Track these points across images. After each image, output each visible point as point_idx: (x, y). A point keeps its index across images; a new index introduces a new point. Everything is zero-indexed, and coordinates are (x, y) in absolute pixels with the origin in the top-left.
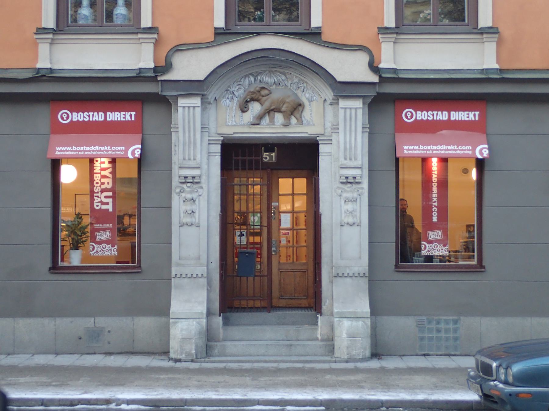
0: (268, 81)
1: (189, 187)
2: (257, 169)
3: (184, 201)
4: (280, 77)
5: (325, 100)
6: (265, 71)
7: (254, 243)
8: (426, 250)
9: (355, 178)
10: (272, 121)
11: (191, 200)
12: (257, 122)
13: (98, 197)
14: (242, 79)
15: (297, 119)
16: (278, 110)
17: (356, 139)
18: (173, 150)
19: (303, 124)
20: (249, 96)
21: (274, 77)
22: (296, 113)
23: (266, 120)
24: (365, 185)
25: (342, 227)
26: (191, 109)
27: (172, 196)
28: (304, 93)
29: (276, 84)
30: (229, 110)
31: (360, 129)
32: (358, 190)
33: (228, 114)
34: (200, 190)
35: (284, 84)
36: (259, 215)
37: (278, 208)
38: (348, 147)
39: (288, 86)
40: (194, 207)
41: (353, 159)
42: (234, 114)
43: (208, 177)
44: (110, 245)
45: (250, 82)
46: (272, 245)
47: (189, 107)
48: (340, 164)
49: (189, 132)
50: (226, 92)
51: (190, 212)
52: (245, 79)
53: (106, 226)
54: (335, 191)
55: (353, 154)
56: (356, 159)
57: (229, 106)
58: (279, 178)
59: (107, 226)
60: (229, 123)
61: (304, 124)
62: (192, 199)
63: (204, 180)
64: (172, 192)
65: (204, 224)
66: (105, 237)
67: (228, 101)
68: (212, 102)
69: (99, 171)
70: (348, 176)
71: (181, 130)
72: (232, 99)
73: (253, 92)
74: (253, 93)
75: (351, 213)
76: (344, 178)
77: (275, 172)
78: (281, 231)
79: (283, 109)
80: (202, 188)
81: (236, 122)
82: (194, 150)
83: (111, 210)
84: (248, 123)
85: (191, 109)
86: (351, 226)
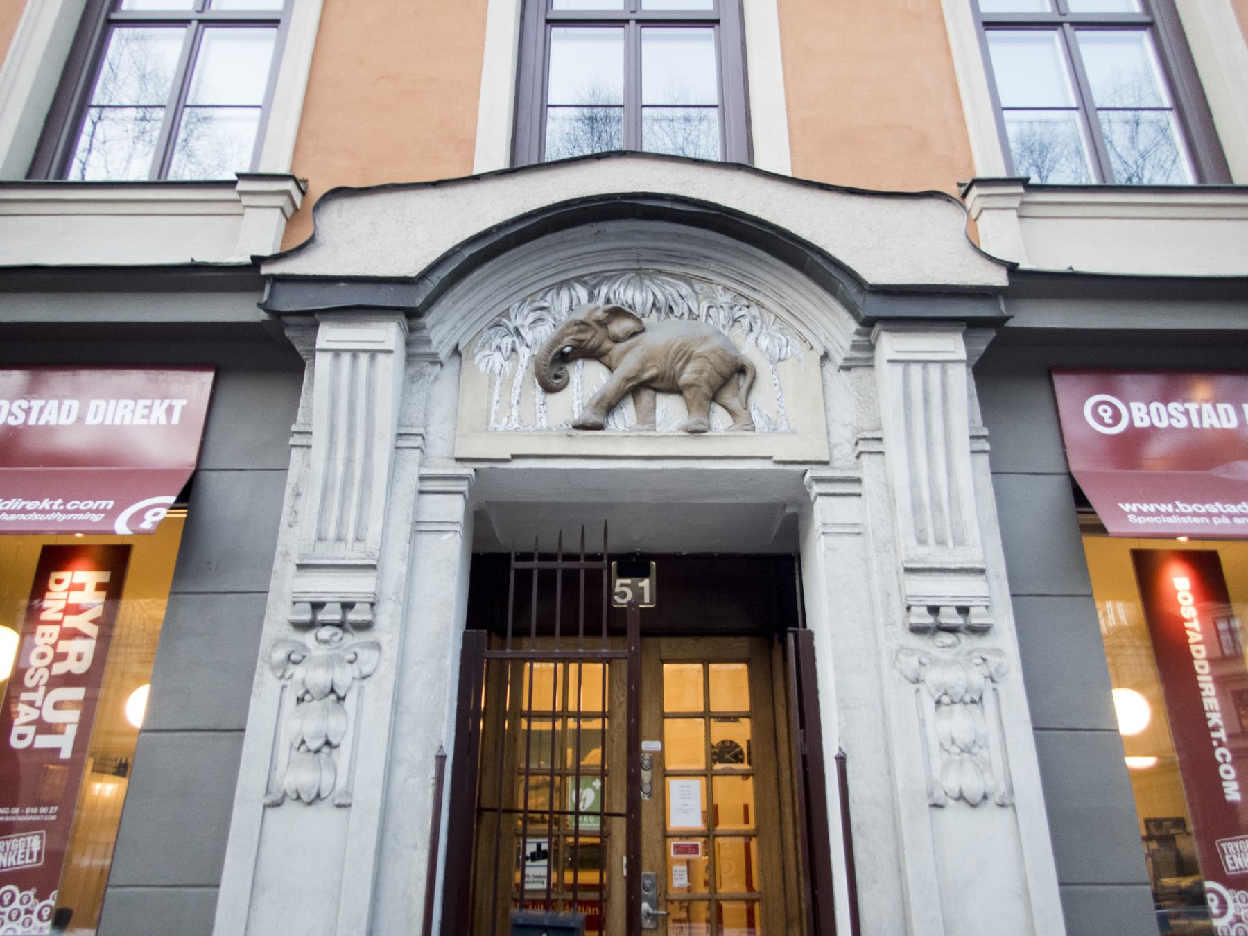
0: (633, 299)
1: (326, 642)
2: (593, 631)
3: (300, 700)
4: (671, 287)
5: (825, 357)
7: (575, 887)
8: (1229, 916)
9: (963, 611)
10: (647, 418)
11: (326, 696)
12: (593, 419)
13: (31, 704)
14: (551, 292)
15: (732, 413)
16: (666, 384)
17: (950, 472)
18: (286, 509)
19: (754, 429)
21: (656, 288)
22: (728, 396)
23: (627, 414)
24: (1005, 637)
25: (935, 810)
26: (364, 359)
27: (256, 678)
28: (753, 336)
29: (659, 310)
31: (962, 442)
32: (984, 660)
33: (496, 397)
34: (364, 655)
35: (685, 306)
36: (597, 783)
37: (660, 757)
38: (926, 498)
39: (698, 316)
40: (336, 725)
41: (950, 542)
43: (407, 609)
44: (31, 893)
46: (640, 891)
47: (355, 353)
48: (904, 558)
49: (351, 443)
50: (492, 331)
51: (314, 745)
52: (558, 294)
53: (33, 814)
54: (895, 661)
55: (948, 522)
56: (959, 542)
58: (663, 661)
59: (38, 814)
60: (497, 426)
62: (332, 691)
63: (386, 618)
64: (259, 663)
65: (368, 797)
66: (20, 856)
67: (498, 358)
68: (442, 356)
69: (59, 616)
70: (937, 603)
71: (319, 441)
72: (514, 353)
73: (582, 323)
74: (583, 327)
75: (966, 750)
76: (925, 610)
77: (651, 641)
78: (672, 843)
79: (687, 377)
80: (377, 646)
81: (521, 422)
82: (361, 506)
83: (66, 754)
84: (565, 426)
85: (364, 359)
86: (973, 806)
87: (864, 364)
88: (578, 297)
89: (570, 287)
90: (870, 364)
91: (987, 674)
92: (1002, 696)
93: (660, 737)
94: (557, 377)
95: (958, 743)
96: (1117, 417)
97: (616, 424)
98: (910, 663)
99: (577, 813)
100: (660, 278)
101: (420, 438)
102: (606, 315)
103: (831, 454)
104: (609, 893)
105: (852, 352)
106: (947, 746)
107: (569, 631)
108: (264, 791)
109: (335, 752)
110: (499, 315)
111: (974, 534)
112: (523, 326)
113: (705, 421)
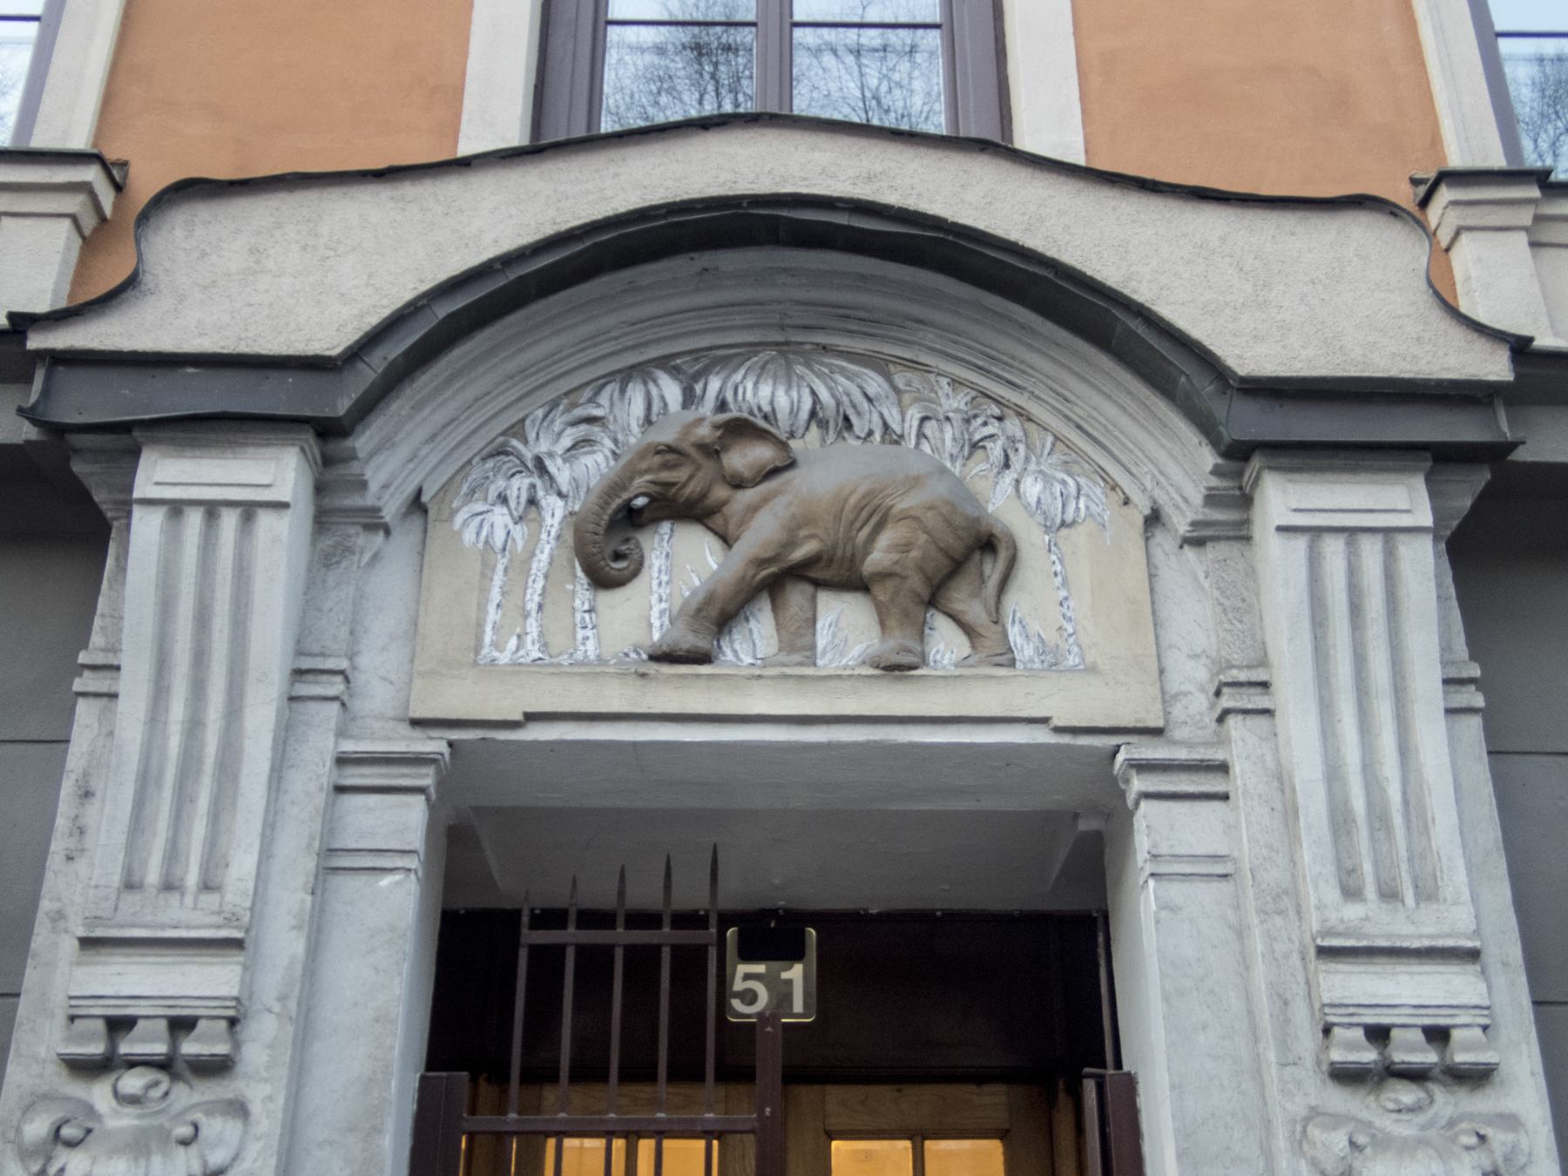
0: (772, 403)
1: (133, 1100)
2: (686, 1072)
4: (848, 378)
5: (1154, 519)
6: (755, 347)
9: (1438, 1035)
12: (689, 640)
14: (609, 388)
17: (1405, 751)
18: (61, 823)
19: (1012, 663)
20: (648, 477)
22: (961, 597)
26: (229, 521)
28: (1009, 477)
29: (823, 425)
30: (506, 570)
32: (1482, 1138)
33: (495, 595)
34: (214, 1127)
38: (1359, 805)
42: (537, 599)
45: (656, 408)
47: (212, 509)
48: (1315, 927)
50: (490, 464)
52: (623, 391)
54: (1300, 1141)
56: (1427, 893)
57: (504, 549)
58: (831, 1136)
60: (496, 654)
61: (1018, 664)
71: (134, 684)
72: (533, 508)
73: (670, 449)
74: (671, 457)
76: (1359, 1034)
79: (879, 557)
80: (239, 1109)
81: (545, 646)
82: (215, 817)
84: (633, 655)
85: (229, 521)
87: (1231, 533)
88: (663, 398)
90: (1244, 533)
94: (618, 556)
97: (735, 652)
100: (827, 360)
101: (339, 679)
102: (718, 433)
105: (1207, 511)
111: (1456, 878)
113: (915, 645)
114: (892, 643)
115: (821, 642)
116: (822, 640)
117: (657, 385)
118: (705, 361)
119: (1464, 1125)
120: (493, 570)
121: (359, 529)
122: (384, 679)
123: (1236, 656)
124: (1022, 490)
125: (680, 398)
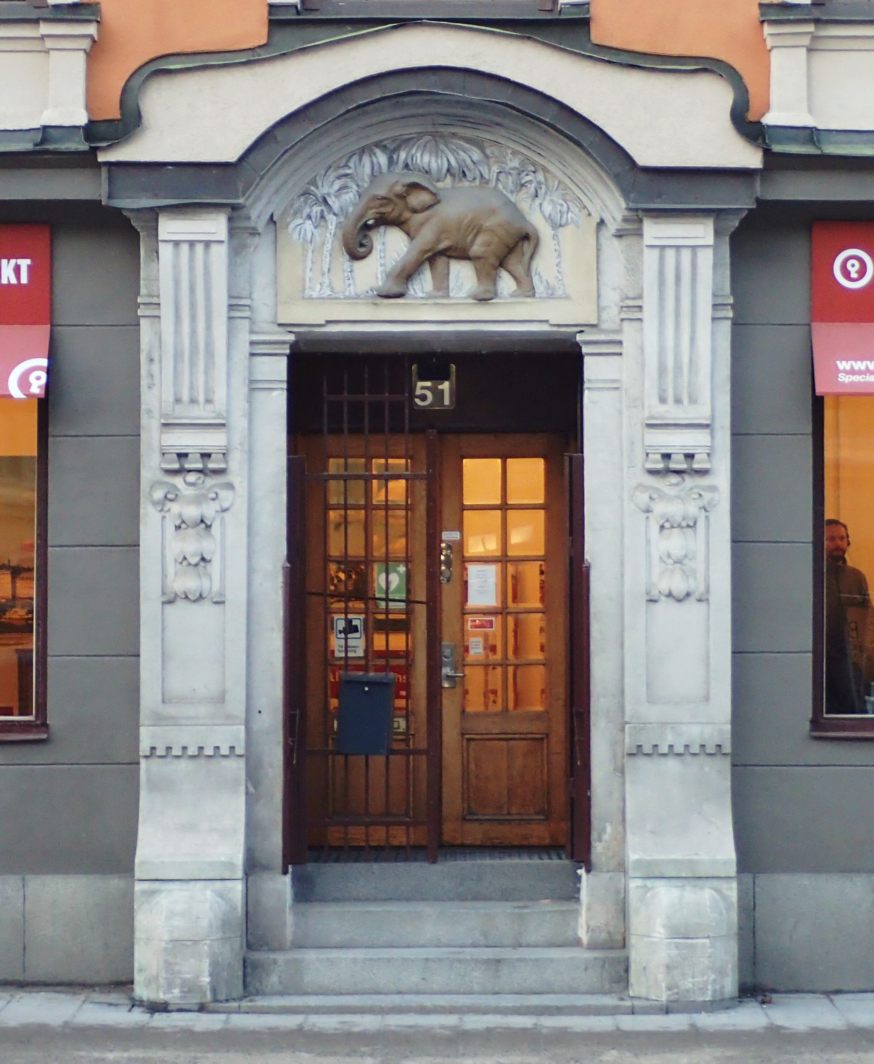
0: (429, 165)
1: (192, 484)
2: (397, 429)
3: (178, 528)
4: (464, 152)
5: (602, 223)
6: (421, 135)
7: (387, 654)
9: (690, 457)
10: (442, 285)
12: (396, 289)
16: (460, 253)
17: (693, 339)
18: (143, 372)
19: (533, 295)
23: (425, 282)
26: (200, 248)
27: (142, 511)
28: (538, 201)
29: (453, 175)
32: (700, 495)
33: (309, 264)
34: (224, 494)
36: (402, 569)
37: (459, 547)
38: (670, 364)
39: (489, 180)
40: (208, 546)
41: (686, 401)
42: (327, 266)
43: (250, 454)
46: (441, 659)
47: (192, 243)
48: (647, 414)
49: (193, 318)
50: (302, 199)
52: (360, 159)
54: (632, 497)
56: (693, 400)
57: (311, 242)
60: (311, 293)
62: (202, 521)
63: (236, 463)
64: (142, 500)
65: (237, 595)
71: (167, 311)
72: (323, 220)
73: (384, 198)
74: (385, 201)
75: (679, 562)
76: (659, 457)
79: (476, 249)
80: (230, 486)
81: (332, 290)
82: (206, 373)
84: (370, 292)
85: (200, 248)
86: (679, 600)
87: (633, 233)
88: (379, 163)
89: (372, 153)
90: (640, 233)
91: (701, 506)
92: (712, 521)
93: (460, 527)
94: (362, 245)
95: (673, 557)
96: (862, 272)
97: (414, 289)
98: (643, 498)
99: (387, 600)
100: (453, 141)
101: (247, 308)
102: (405, 188)
103: (599, 318)
104: (413, 660)
105: (623, 224)
106: (665, 559)
107: (376, 429)
108: (160, 593)
109: (208, 566)
110: (308, 183)
111: (705, 395)
112: (329, 194)
113: (491, 288)
114: (482, 289)
115: (451, 285)
116: (452, 284)
117: (376, 157)
118: (397, 142)
119: (695, 490)
120: (307, 251)
121: (248, 235)
122: (265, 304)
123: (630, 293)
124: (542, 209)
125: (387, 163)
